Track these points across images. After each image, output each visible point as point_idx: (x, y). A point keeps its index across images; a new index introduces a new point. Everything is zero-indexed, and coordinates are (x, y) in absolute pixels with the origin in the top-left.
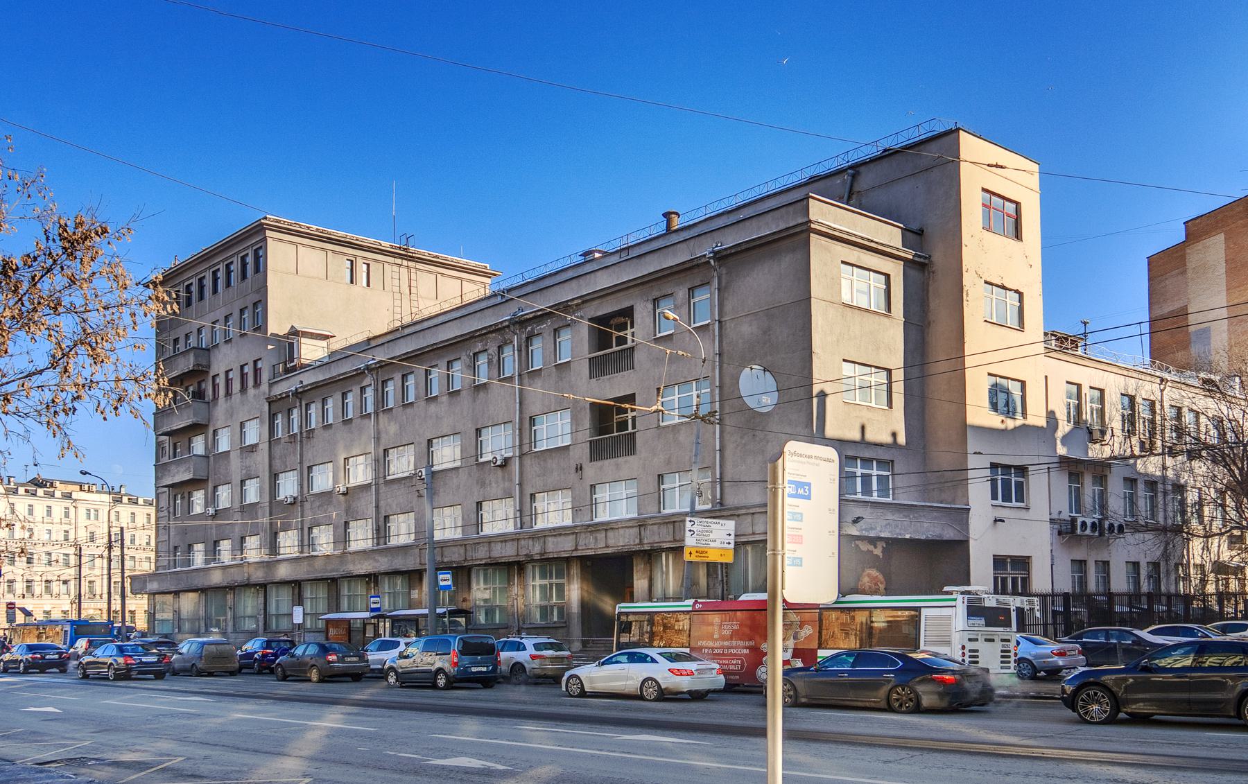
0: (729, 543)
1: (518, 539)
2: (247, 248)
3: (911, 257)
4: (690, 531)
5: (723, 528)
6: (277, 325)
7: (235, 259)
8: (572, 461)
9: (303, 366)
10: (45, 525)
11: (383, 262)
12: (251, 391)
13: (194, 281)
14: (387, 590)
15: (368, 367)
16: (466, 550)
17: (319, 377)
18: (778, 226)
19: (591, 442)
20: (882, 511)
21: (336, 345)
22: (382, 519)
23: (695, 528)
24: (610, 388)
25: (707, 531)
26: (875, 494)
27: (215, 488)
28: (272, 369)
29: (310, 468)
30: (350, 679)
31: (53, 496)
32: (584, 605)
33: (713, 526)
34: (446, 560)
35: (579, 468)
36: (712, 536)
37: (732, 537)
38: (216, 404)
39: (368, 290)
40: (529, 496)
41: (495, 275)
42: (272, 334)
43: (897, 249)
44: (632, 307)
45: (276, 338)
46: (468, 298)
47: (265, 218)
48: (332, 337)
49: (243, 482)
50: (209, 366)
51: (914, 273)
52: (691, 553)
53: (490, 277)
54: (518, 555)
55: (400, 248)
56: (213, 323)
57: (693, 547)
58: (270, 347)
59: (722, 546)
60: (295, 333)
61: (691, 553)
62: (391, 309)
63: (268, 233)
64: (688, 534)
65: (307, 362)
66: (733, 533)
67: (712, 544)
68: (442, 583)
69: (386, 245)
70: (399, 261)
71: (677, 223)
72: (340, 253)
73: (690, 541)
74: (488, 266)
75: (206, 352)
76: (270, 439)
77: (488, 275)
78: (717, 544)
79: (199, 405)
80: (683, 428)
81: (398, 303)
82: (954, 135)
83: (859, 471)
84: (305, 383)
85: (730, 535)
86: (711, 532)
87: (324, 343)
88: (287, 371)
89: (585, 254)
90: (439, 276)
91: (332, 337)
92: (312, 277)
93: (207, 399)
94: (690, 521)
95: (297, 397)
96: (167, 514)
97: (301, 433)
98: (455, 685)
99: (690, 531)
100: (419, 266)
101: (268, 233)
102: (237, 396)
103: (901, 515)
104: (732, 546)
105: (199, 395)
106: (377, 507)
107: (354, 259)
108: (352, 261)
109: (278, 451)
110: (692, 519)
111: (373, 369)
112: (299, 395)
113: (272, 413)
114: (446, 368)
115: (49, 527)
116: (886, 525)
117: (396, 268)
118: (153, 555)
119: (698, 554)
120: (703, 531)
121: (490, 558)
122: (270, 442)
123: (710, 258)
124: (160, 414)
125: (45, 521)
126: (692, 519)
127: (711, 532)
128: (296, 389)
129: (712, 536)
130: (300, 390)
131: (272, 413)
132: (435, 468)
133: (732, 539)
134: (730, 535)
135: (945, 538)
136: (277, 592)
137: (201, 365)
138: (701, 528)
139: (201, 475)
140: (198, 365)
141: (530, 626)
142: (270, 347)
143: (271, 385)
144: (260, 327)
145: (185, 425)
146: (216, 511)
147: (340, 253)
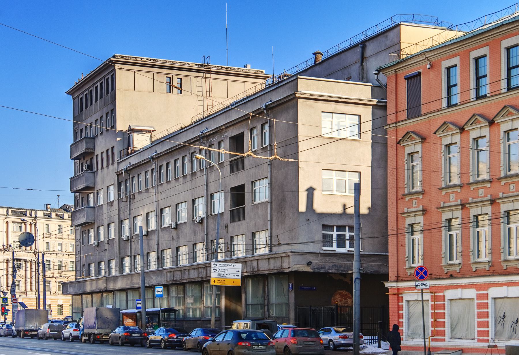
0: (238, 276)
1: (198, 268)
2: (107, 75)
3: (375, 103)
4: (214, 269)
5: (234, 267)
6: (121, 126)
7: (103, 80)
8: (224, 222)
9: (135, 151)
10: (57, 240)
11: (190, 77)
12: (111, 167)
13: (98, 84)
14: (190, 294)
15: (152, 158)
16: (181, 273)
17: (147, 156)
18: (253, 110)
19: (231, 210)
20: (329, 258)
21: (159, 135)
22: (160, 252)
23: (217, 268)
24: (236, 181)
25: (224, 270)
26: (347, 191)
27: (98, 227)
28: (119, 153)
29: (134, 218)
30: (53, 339)
31: (62, 218)
32: (226, 308)
33: (228, 267)
34: (175, 279)
35: (227, 227)
36: (227, 272)
37: (240, 272)
38: (97, 174)
39: (180, 96)
40: (210, 242)
41: (268, 77)
42: (119, 131)
43: (370, 101)
44: (243, 133)
45: (122, 133)
46: (250, 92)
47: (114, 57)
48: (153, 131)
49: (109, 225)
50: (94, 149)
51: (379, 113)
52: (214, 281)
53: (265, 79)
54: (198, 278)
55: (202, 65)
56: (90, 124)
57: (216, 278)
58: (118, 139)
59: (234, 277)
60: (131, 130)
61: (214, 281)
62: (196, 108)
63: (116, 66)
64: (212, 271)
65: (137, 149)
66: (240, 270)
67: (227, 276)
68: (157, 293)
69: (192, 65)
70: (201, 74)
71: (320, 58)
72: (162, 73)
73: (214, 275)
74: (264, 71)
75: (93, 140)
76: (118, 198)
77: (264, 78)
78: (231, 276)
79: (89, 175)
80: (259, 205)
81: (201, 103)
82: (396, 30)
83: (335, 234)
84: (158, 152)
85: (238, 271)
86: (227, 270)
87: (149, 135)
88: (128, 154)
89: (280, 77)
90: (229, 81)
91: (153, 131)
92: (144, 91)
93: (94, 170)
94: (214, 264)
95: (128, 173)
96: (79, 244)
97: (130, 196)
98: (124, 345)
99: (214, 269)
100: (213, 76)
101: (116, 66)
102: (105, 169)
103: (345, 260)
104: (240, 277)
105: (90, 167)
106: (158, 244)
107: (171, 76)
108: (170, 78)
109: (122, 204)
110: (215, 263)
111: (155, 159)
112: (129, 172)
113: (119, 182)
114: (217, 148)
115: (60, 241)
116: (333, 266)
117: (199, 80)
118: (205, 252)
119: (219, 282)
120: (222, 270)
121: (189, 278)
122: (118, 200)
123: (264, 109)
124: (73, 180)
125: (57, 236)
126: (215, 263)
127: (227, 270)
128: (127, 168)
129: (227, 272)
130: (128, 169)
131: (119, 182)
132: (179, 222)
133: (240, 274)
134: (238, 271)
135: (381, 273)
136: (120, 296)
137: (89, 149)
138: (221, 268)
139: (91, 219)
140: (88, 148)
141: (205, 319)
142: (118, 139)
143: (119, 164)
144: (114, 126)
145: (83, 187)
146: (98, 243)
147: (162, 73)
